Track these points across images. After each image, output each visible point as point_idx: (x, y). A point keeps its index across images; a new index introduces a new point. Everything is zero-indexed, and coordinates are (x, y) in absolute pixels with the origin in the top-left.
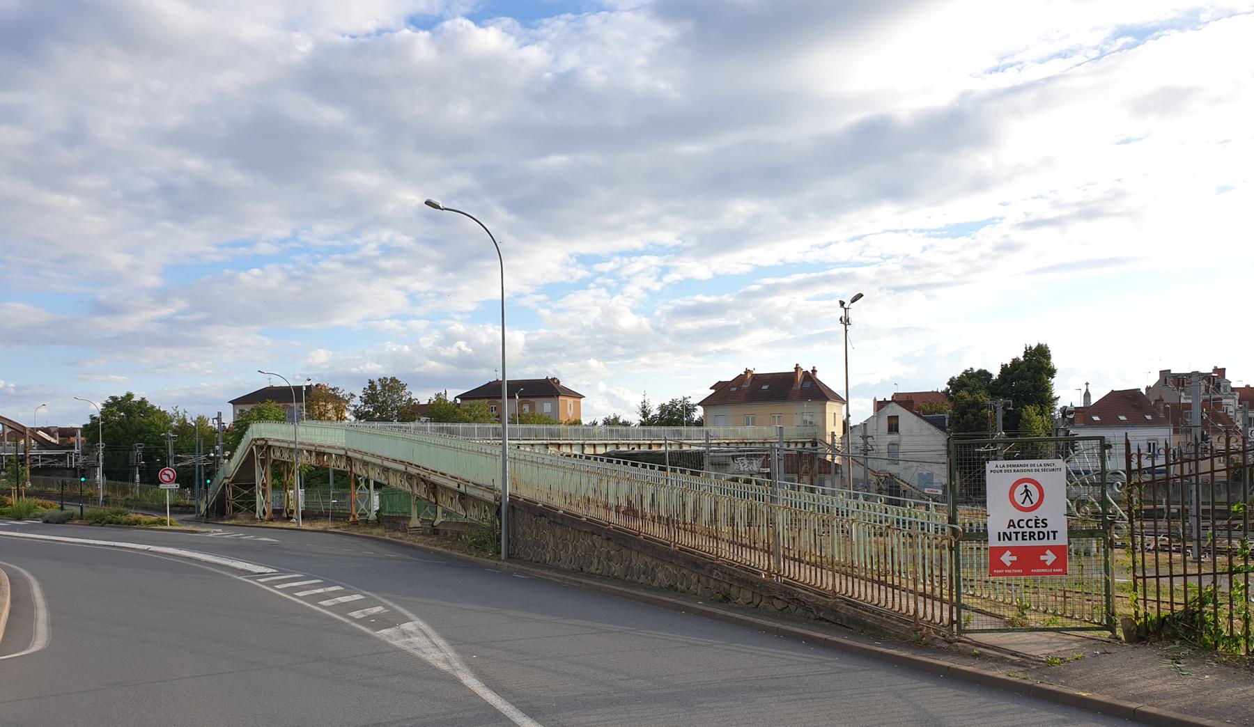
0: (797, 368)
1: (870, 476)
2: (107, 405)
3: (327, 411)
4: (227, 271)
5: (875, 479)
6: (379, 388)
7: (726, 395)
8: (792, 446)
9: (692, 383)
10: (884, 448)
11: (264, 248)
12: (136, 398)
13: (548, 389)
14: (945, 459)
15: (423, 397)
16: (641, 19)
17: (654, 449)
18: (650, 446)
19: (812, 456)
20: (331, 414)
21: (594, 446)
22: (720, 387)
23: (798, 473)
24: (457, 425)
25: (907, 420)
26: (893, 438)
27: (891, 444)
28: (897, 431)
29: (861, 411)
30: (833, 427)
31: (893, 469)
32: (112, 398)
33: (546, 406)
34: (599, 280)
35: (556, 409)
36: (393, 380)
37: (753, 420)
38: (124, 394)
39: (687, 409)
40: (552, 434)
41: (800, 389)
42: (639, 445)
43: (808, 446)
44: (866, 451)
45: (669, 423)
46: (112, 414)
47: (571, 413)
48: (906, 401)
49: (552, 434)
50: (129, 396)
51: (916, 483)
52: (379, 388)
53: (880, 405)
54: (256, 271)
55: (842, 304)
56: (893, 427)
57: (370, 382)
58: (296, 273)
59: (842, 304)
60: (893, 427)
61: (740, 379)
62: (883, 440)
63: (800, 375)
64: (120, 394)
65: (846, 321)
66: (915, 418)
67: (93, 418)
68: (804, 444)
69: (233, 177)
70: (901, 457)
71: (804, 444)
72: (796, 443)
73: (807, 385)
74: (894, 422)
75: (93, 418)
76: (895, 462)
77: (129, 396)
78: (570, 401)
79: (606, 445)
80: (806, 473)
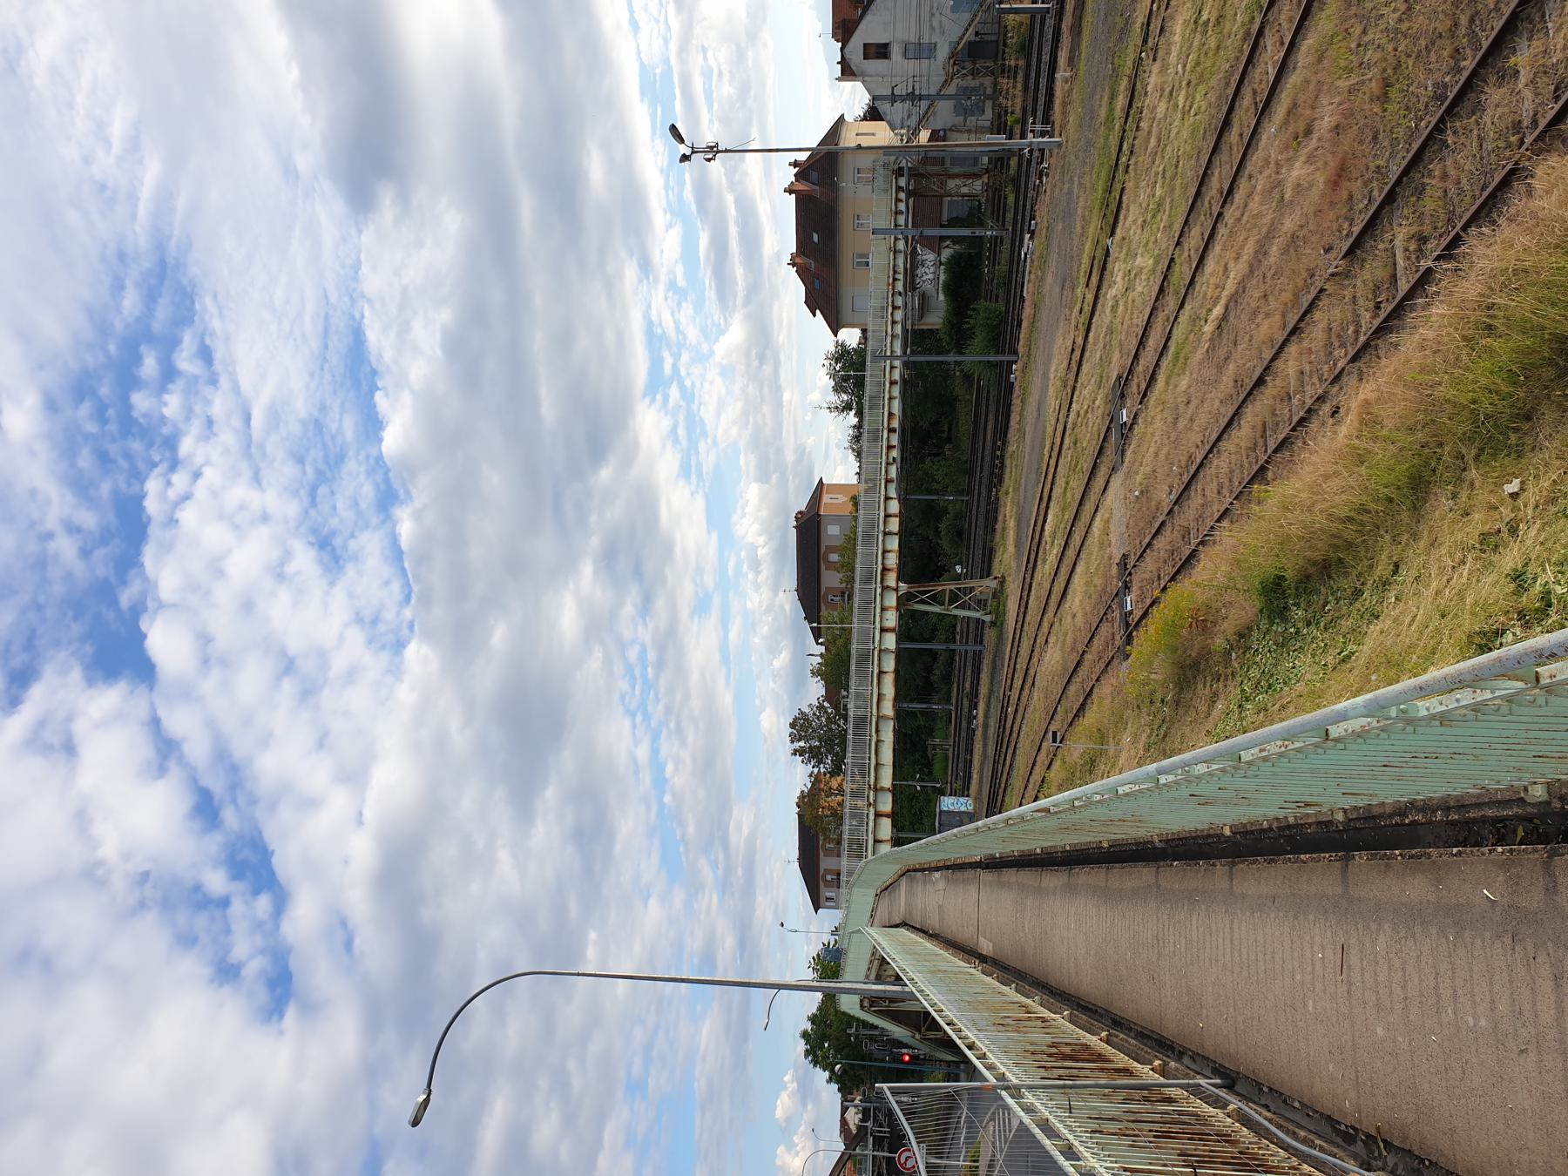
0: (789, 191)
1: (951, 90)
2: (815, 1063)
3: (830, 808)
4: (667, 799)
5: (955, 81)
6: (802, 744)
7: (825, 298)
8: (899, 301)
9: (811, 342)
10: (911, 66)
11: (642, 753)
12: (808, 1026)
13: (809, 526)
14: (973, 890)
15: (815, 690)
16: (367, 237)
17: (895, 424)
18: (891, 430)
19: (914, 174)
20: (834, 800)
21: (887, 516)
22: (813, 303)
23: (941, 196)
24: (853, 652)
25: (870, 30)
26: (896, 52)
27: (905, 55)
28: (886, 46)
29: (854, 98)
30: (882, 135)
31: (943, 52)
32: (806, 1056)
33: (832, 531)
34: (683, 372)
35: (837, 519)
36: (792, 725)
37: (861, 256)
38: (803, 1042)
39: (842, 355)
40: (868, 579)
41: (820, 179)
42: (890, 447)
43: (902, 182)
44: (912, 97)
45: (860, 383)
46: (825, 1058)
47: (842, 499)
48: (844, 29)
49: (868, 579)
50: (805, 1035)
51: (967, 17)
52: (802, 744)
53: (847, 71)
54: (669, 768)
55: (685, 158)
56: (879, 51)
57: (795, 752)
58: (672, 725)
59: (685, 158)
60: (879, 51)
61: (803, 273)
62: (899, 67)
63: (800, 187)
64: (801, 1046)
65: (713, 151)
66: (868, 17)
67: (830, 1080)
68: (899, 189)
69: (566, 759)
70: (926, 40)
71: (899, 189)
72: (898, 200)
73: (814, 175)
74: (873, 50)
75: (830, 1080)
76: (933, 48)
77: (805, 1035)
78: (826, 499)
79: (887, 498)
80: (943, 184)
